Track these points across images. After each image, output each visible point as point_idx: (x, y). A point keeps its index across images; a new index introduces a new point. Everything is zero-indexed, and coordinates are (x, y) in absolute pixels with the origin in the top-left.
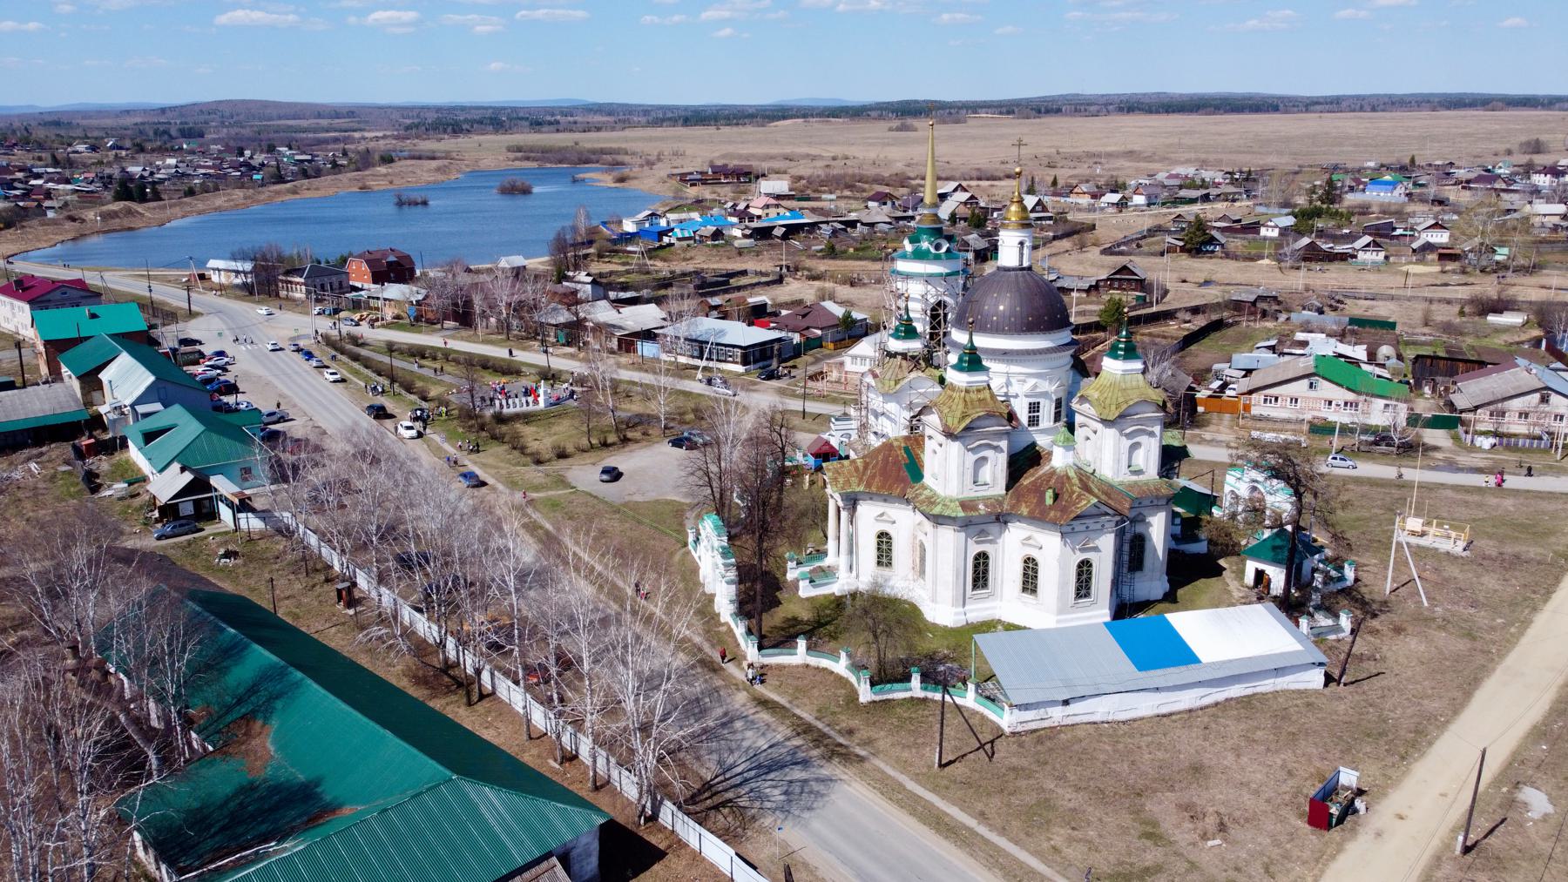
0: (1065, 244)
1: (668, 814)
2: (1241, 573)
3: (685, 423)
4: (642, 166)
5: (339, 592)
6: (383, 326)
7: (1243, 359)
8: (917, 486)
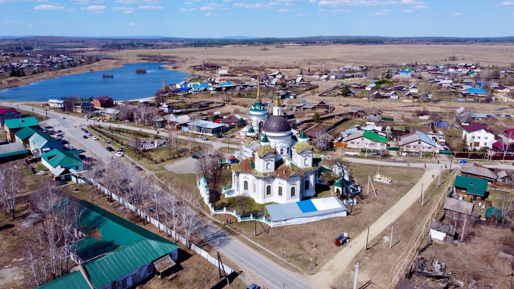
0: (309, 92)
1: (193, 247)
2: (334, 190)
3: (196, 151)
4: (181, 62)
5: (108, 199)
6: (106, 122)
7: (348, 131)
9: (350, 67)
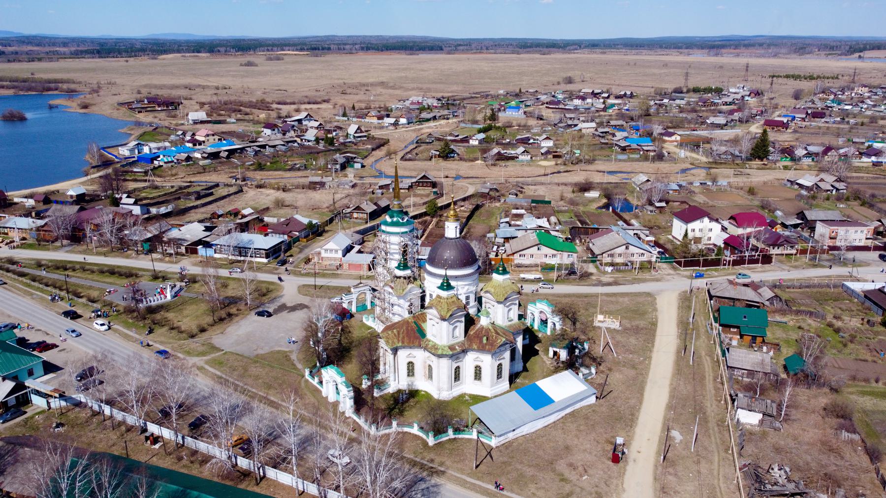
2: (547, 351)
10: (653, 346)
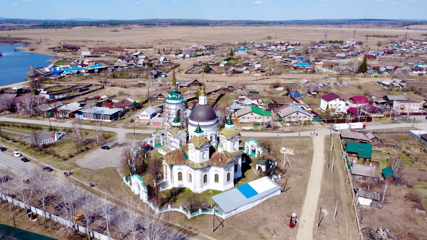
2: (255, 167)
4: (36, 44)
8: (187, 160)
9: (197, 46)
10: (312, 163)
